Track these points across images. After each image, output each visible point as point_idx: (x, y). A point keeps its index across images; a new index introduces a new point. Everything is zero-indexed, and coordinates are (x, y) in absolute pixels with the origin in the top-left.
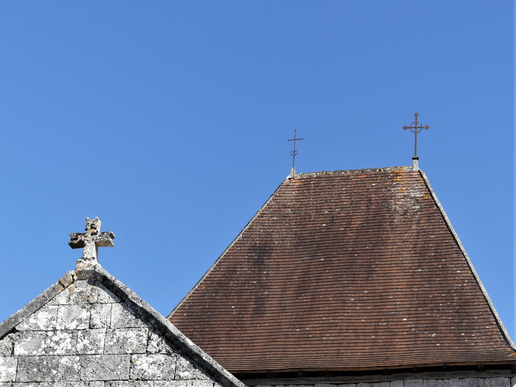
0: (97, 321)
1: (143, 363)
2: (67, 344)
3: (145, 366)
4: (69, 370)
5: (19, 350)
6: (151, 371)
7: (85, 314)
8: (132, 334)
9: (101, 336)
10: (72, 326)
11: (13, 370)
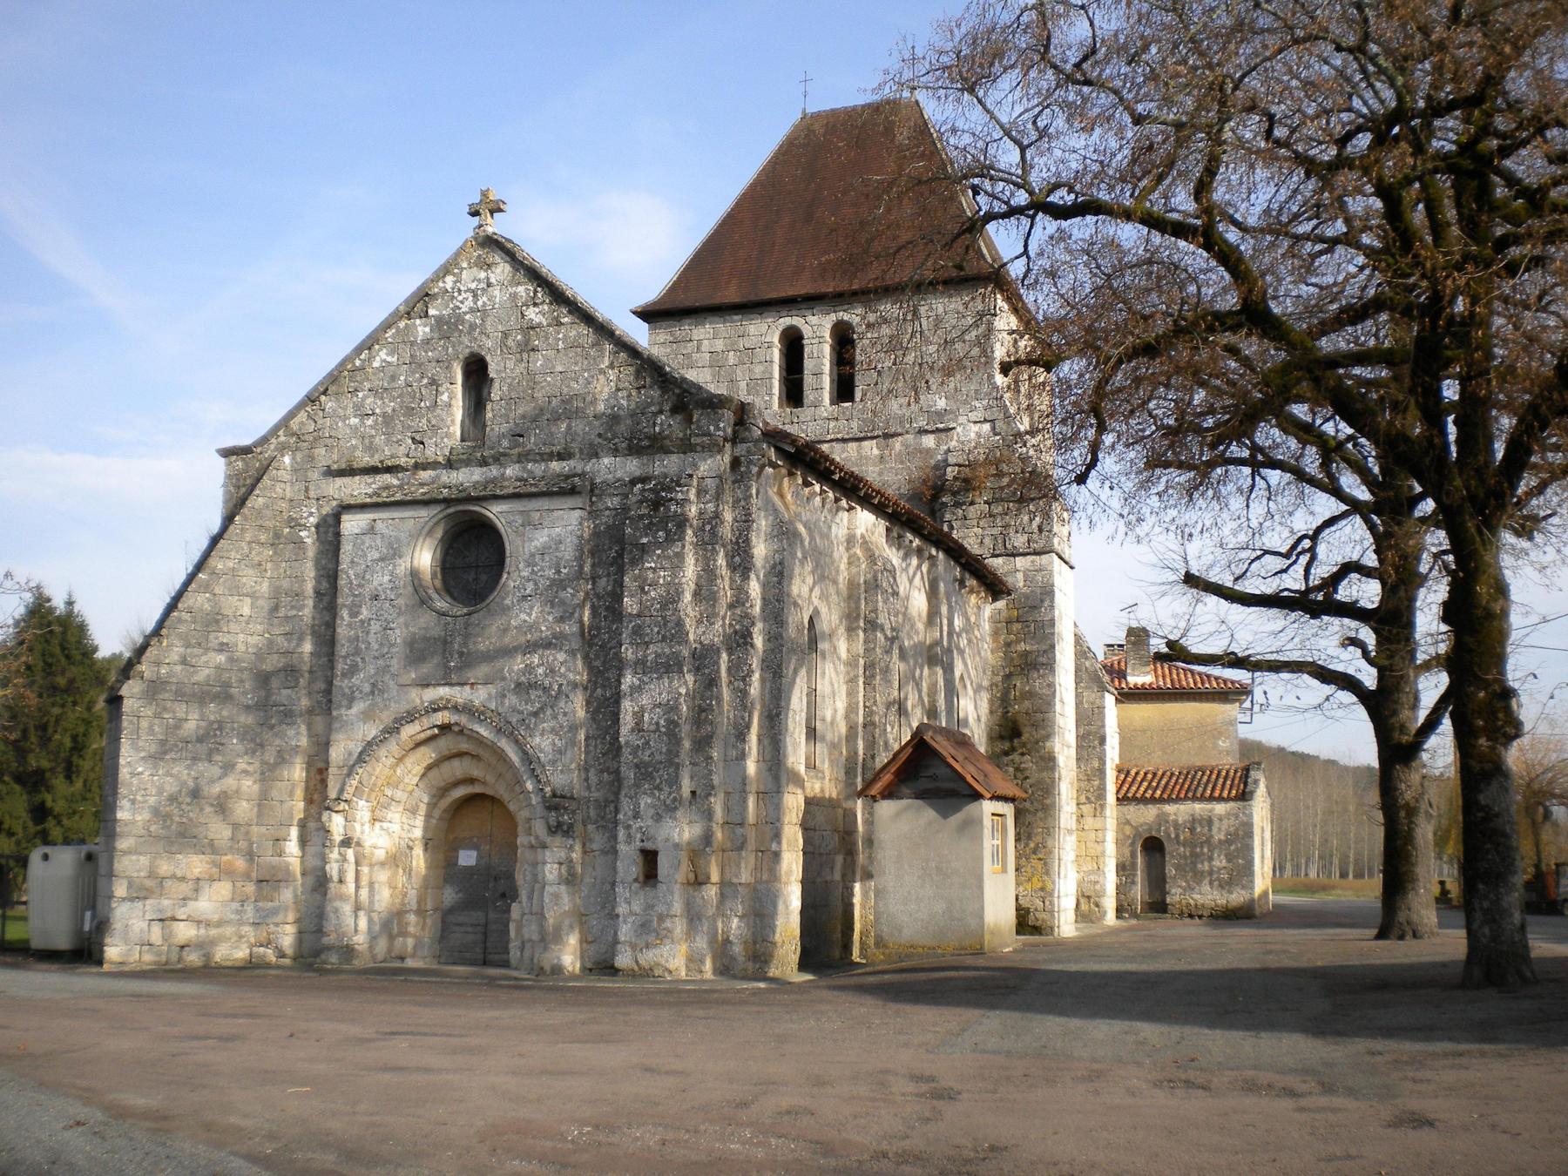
0: (493, 280)
1: (532, 314)
2: (470, 303)
3: (533, 316)
4: (473, 327)
5: (432, 312)
6: (537, 319)
7: (483, 275)
8: (521, 289)
9: (497, 293)
10: (473, 286)
11: (427, 329)
